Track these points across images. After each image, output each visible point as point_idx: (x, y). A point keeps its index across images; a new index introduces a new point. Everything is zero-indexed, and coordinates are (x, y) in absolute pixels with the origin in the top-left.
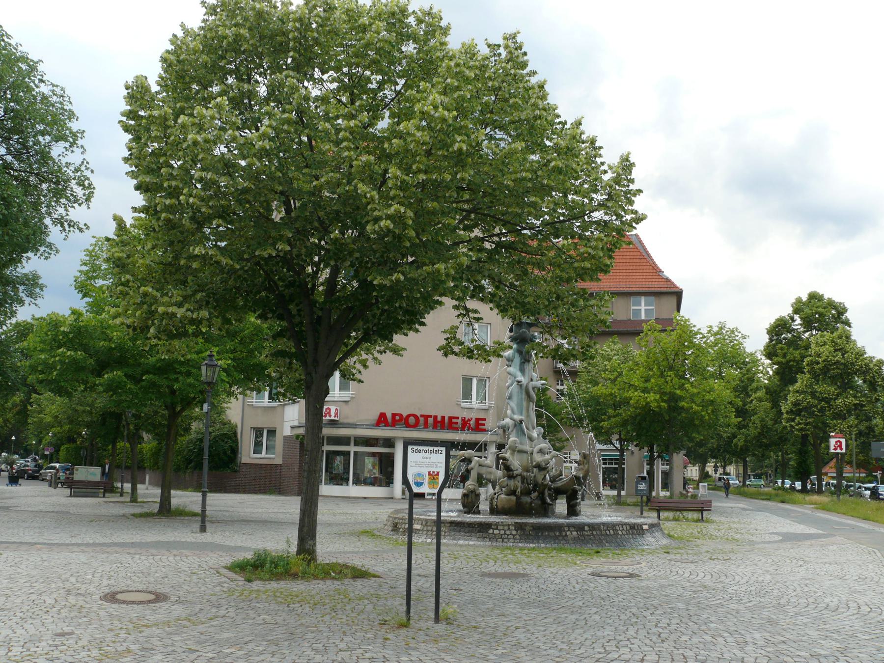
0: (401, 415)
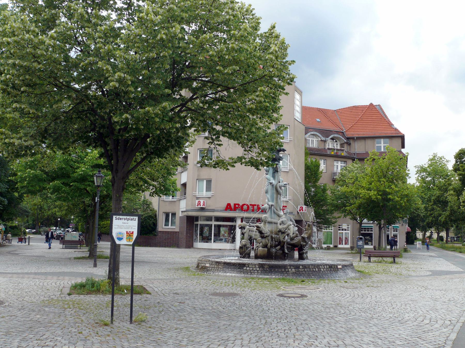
0: (238, 205)
